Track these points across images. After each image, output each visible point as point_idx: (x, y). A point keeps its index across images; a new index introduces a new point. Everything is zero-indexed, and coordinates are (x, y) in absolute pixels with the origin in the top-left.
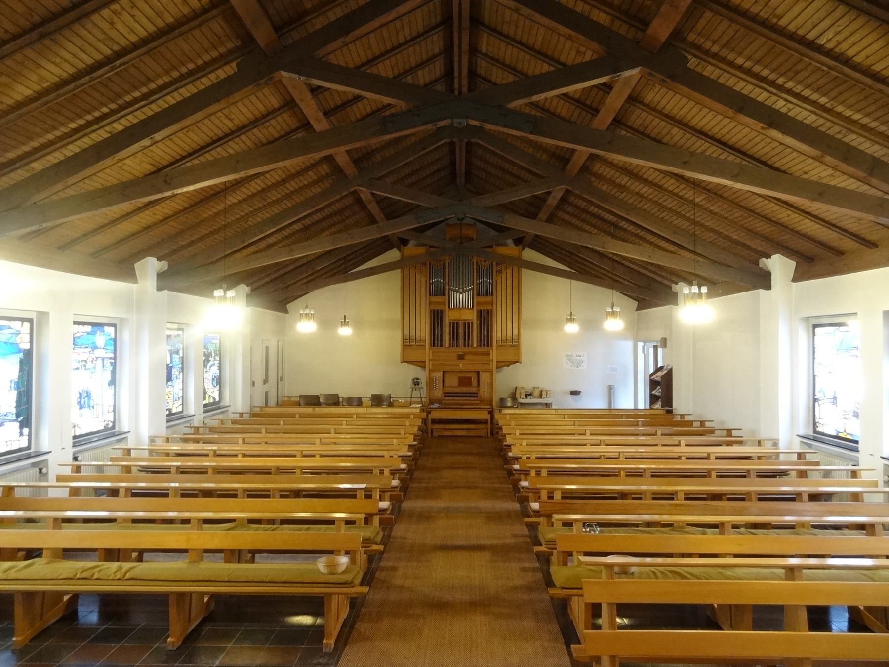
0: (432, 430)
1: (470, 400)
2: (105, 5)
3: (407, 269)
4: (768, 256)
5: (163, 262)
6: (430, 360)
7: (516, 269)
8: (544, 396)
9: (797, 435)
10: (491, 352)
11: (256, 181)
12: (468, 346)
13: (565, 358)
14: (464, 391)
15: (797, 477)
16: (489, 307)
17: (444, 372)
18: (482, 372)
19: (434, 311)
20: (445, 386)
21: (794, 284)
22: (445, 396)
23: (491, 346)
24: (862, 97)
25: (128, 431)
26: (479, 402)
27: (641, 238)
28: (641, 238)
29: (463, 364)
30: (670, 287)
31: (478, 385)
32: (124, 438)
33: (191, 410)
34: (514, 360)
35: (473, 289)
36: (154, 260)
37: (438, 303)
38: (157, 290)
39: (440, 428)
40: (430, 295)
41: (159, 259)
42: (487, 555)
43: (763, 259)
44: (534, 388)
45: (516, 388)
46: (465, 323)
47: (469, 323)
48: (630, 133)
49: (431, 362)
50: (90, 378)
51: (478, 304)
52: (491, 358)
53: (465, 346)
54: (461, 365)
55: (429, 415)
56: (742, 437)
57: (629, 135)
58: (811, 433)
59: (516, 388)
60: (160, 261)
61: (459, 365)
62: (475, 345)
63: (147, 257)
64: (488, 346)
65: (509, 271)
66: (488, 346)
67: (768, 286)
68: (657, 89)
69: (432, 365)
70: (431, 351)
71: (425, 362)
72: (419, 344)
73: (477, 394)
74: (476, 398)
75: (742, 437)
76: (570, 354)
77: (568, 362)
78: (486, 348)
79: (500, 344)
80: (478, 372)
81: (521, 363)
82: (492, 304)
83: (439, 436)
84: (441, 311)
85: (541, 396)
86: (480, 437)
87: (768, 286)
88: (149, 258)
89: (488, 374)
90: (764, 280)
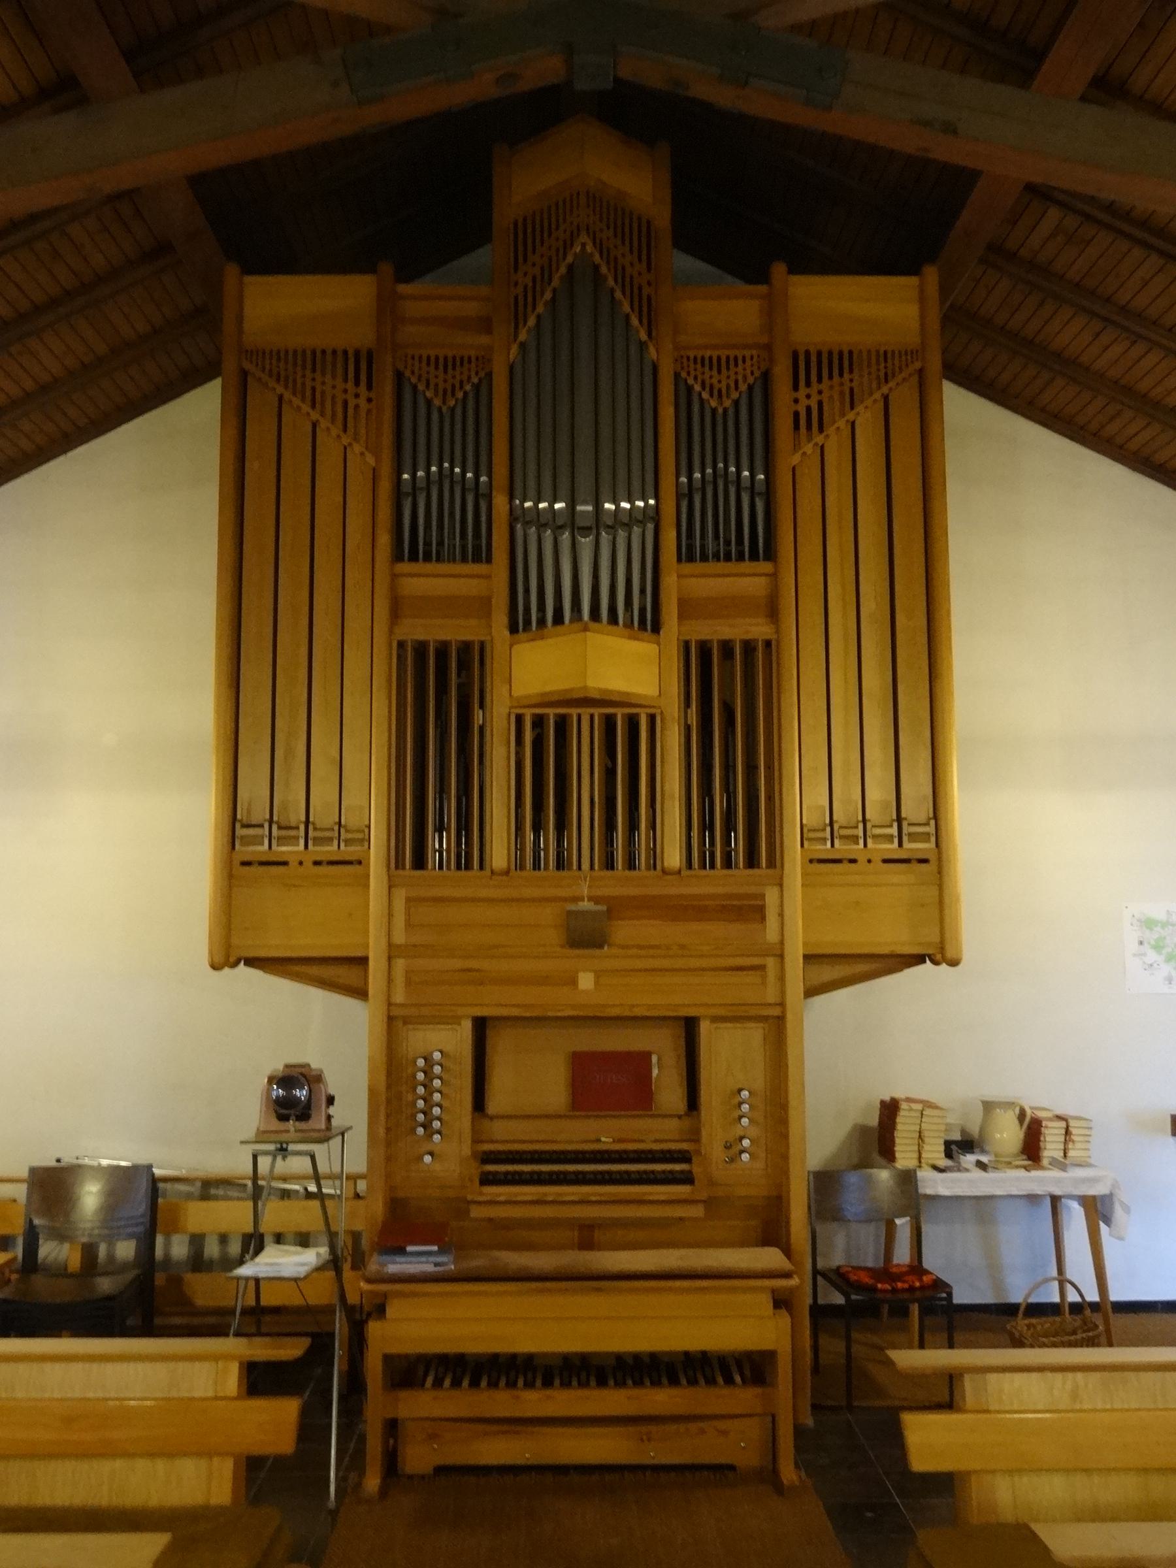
0: (392, 1426)
1: (641, 1202)
3: (260, 401)
6: (393, 952)
7: (904, 396)
8: (1051, 1147)
10: (771, 897)
12: (631, 864)
13: (1131, 936)
14: (607, 1142)
15: (562, 946)
16: (759, 629)
17: (481, 1026)
18: (715, 1019)
19: (421, 649)
20: (492, 1107)
22: (487, 1180)
23: (771, 864)
26: (698, 1211)
29: (598, 974)
31: (693, 1102)
34: (899, 940)
35: (655, 516)
37: (449, 606)
39: (452, 1412)
40: (398, 557)
44: (989, 1107)
45: (890, 1109)
46: (609, 723)
47: (633, 723)
49: (400, 964)
50: (1133, 916)
51: (687, 609)
52: (772, 934)
53: (609, 864)
54: (586, 981)
55: (374, 1328)
59: (890, 1109)
61: (573, 982)
62: (673, 857)
64: (752, 861)
65: (867, 418)
66: (752, 861)
69: (408, 983)
70: (400, 895)
71: (363, 961)
72: (329, 850)
73: (685, 1157)
74: (682, 1190)
76: (1161, 916)
77: (1152, 956)
78: (719, 872)
79: (823, 849)
80: (690, 1026)
81: (954, 963)
82: (773, 612)
83: (441, 1470)
84: (465, 648)
85: (1031, 1149)
86: (721, 1472)
89: (755, 1034)
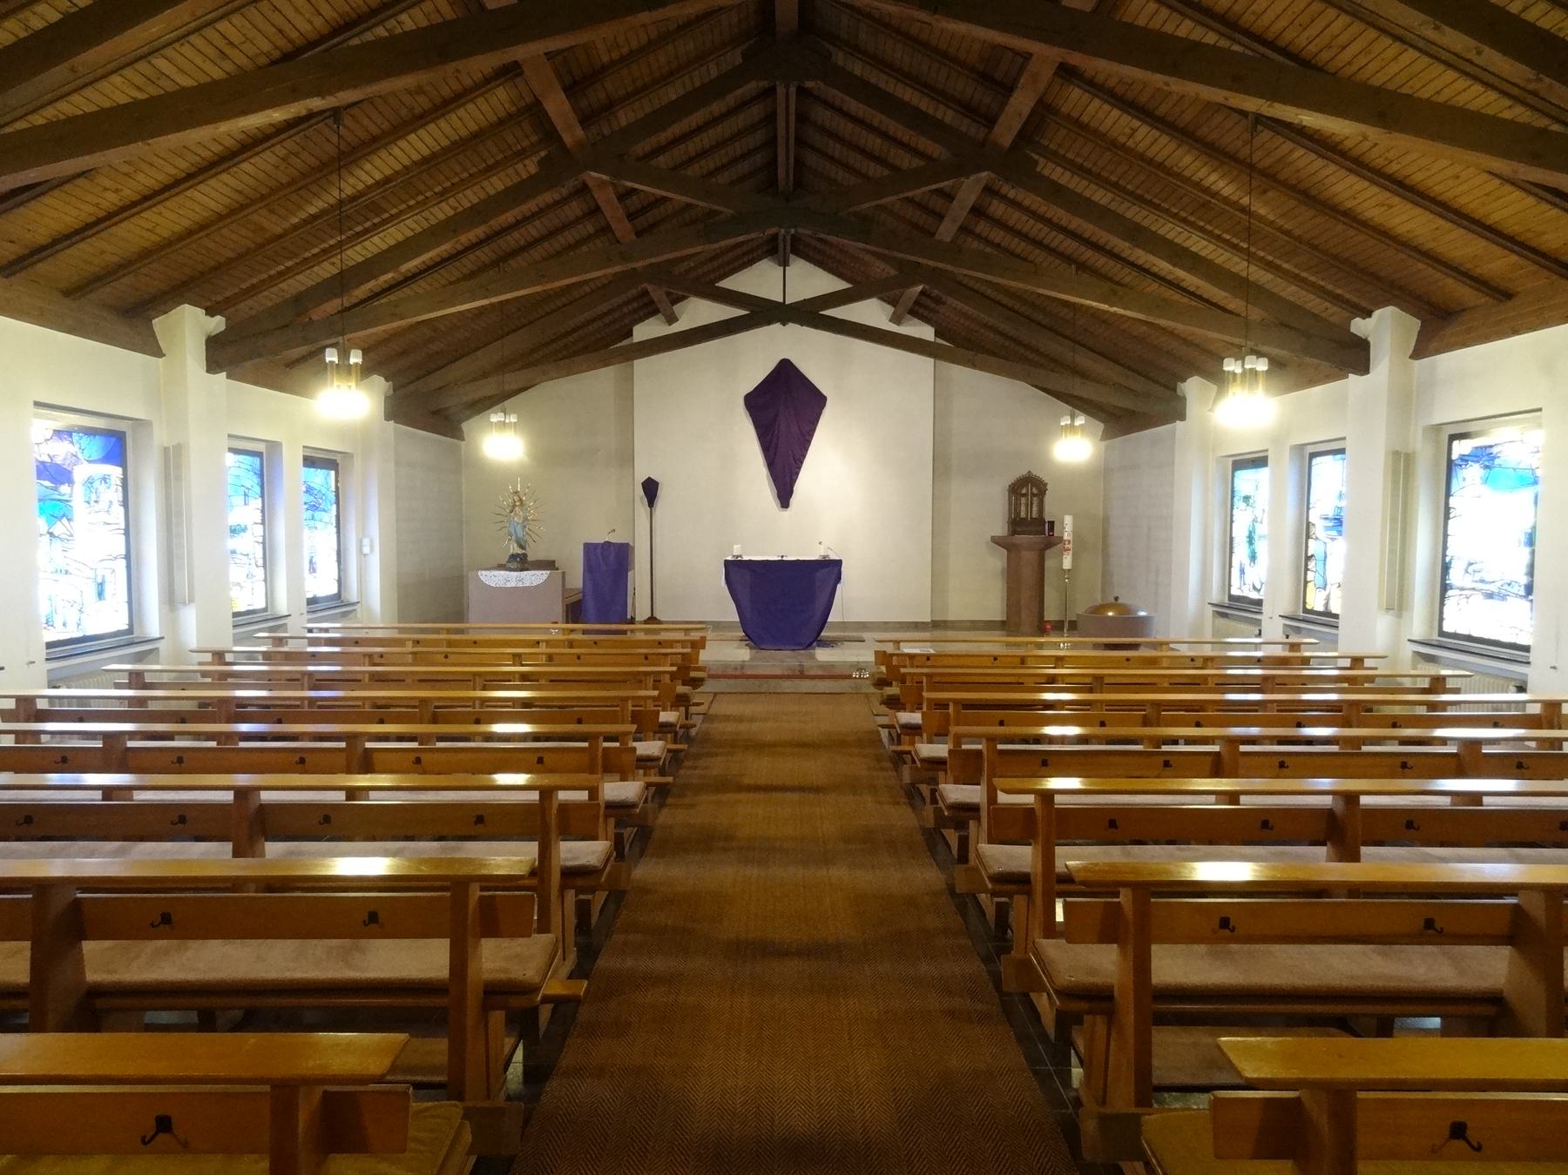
2: (23, 7)
4: (1367, 314)
5: (218, 318)
9: (1409, 640)
11: (399, 143)
21: (1417, 363)
24: (263, 168)
25: (158, 636)
27: (1082, 266)
28: (1082, 266)
30: (937, 334)
32: (151, 651)
33: (282, 606)
36: (200, 312)
38: (208, 371)
41: (211, 312)
42: (746, 781)
43: (1358, 319)
48: (1240, 44)
56: (1376, 669)
57: (1236, 48)
58: (1435, 637)
60: (212, 316)
63: (183, 303)
67: (1363, 367)
68: (507, 106)
75: (1376, 669)
87: (1363, 367)
88: (186, 306)
90: (1355, 357)
